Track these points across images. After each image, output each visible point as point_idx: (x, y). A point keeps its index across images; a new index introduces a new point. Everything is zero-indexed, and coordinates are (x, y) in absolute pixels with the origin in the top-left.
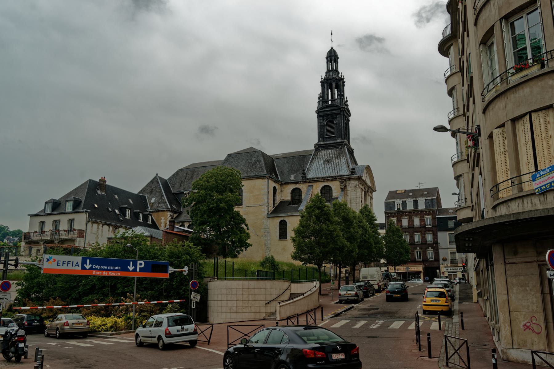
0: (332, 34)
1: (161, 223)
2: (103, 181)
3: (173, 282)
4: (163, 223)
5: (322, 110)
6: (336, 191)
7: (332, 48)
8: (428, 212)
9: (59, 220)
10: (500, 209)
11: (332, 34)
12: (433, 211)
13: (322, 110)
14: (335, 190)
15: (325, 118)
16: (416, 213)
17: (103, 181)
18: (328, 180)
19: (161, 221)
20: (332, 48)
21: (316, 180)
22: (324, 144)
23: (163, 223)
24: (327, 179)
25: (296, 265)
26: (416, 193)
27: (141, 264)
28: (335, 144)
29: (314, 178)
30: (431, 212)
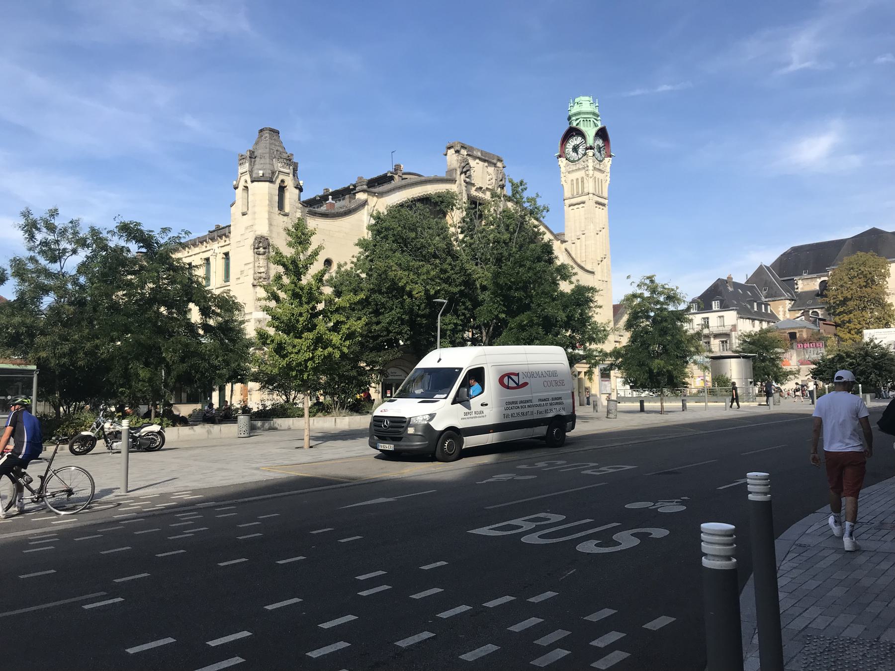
1: (779, 311)
2: (730, 278)
17: (730, 278)
19: (779, 309)
23: (781, 311)
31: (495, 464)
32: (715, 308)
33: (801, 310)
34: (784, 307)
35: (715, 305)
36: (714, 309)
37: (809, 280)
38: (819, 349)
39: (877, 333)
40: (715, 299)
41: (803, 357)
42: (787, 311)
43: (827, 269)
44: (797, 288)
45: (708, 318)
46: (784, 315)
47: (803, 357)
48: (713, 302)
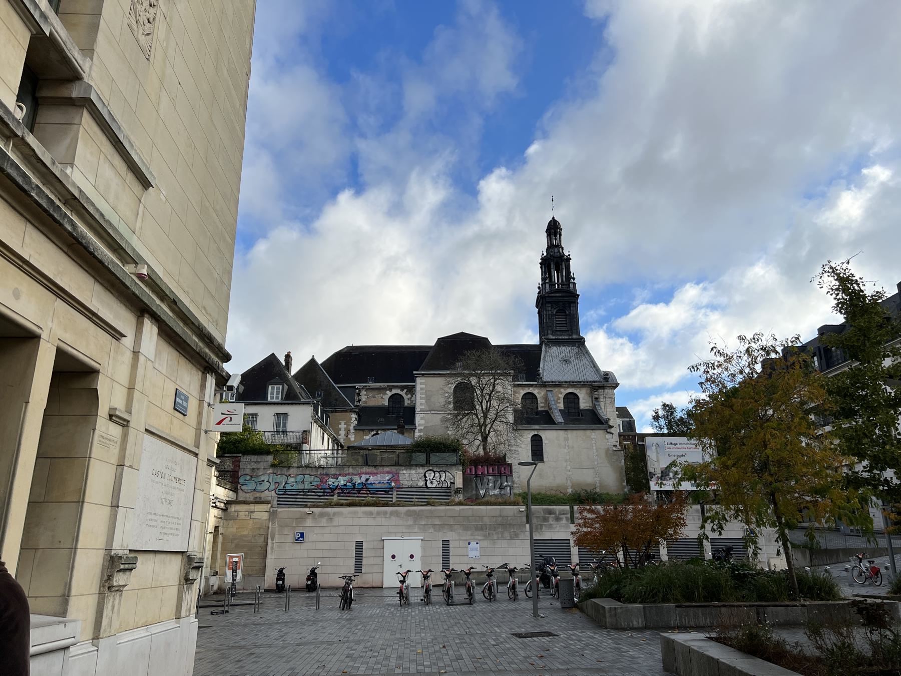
0: (553, 200)
1: (340, 429)
2: (562, 229)
3: (823, 420)
4: (343, 429)
5: (550, 295)
6: (584, 401)
7: (553, 218)
8: (626, 437)
9: (61, 354)
10: (117, 602)
11: (553, 200)
12: (633, 436)
13: (550, 295)
14: (583, 399)
15: (554, 305)
16: (626, 437)
17: (562, 229)
18: (573, 386)
19: (340, 426)
20: (553, 218)
21: (559, 385)
22: (556, 339)
23: (343, 429)
24: (571, 384)
25: (582, 494)
26: (104, 558)
27: (298, 535)
28: (569, 341)
29: (555, 382)
30: (631, 437)
31: (137, 321)
32: (272, 398)
33: (372, 430)
34: (348, 424)
35: (272, 393)
36: (269, 399)
37: (376, 392)
38: (504, 478)
39: (669, 446)
40: (272, 381)
41: (474, 492)
42: (352, 431)
43: (414, 372)
44: (359, 401)
45: (286, 415)
46: (347, 436)
47: (474, 492)
48: (270, 387)
